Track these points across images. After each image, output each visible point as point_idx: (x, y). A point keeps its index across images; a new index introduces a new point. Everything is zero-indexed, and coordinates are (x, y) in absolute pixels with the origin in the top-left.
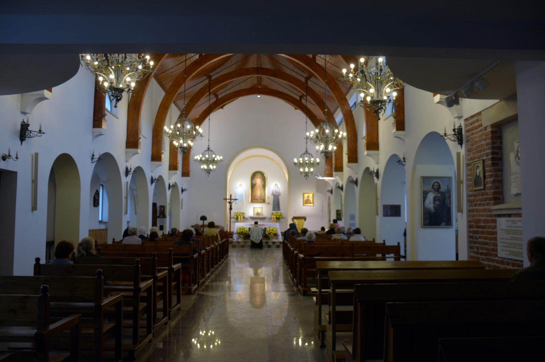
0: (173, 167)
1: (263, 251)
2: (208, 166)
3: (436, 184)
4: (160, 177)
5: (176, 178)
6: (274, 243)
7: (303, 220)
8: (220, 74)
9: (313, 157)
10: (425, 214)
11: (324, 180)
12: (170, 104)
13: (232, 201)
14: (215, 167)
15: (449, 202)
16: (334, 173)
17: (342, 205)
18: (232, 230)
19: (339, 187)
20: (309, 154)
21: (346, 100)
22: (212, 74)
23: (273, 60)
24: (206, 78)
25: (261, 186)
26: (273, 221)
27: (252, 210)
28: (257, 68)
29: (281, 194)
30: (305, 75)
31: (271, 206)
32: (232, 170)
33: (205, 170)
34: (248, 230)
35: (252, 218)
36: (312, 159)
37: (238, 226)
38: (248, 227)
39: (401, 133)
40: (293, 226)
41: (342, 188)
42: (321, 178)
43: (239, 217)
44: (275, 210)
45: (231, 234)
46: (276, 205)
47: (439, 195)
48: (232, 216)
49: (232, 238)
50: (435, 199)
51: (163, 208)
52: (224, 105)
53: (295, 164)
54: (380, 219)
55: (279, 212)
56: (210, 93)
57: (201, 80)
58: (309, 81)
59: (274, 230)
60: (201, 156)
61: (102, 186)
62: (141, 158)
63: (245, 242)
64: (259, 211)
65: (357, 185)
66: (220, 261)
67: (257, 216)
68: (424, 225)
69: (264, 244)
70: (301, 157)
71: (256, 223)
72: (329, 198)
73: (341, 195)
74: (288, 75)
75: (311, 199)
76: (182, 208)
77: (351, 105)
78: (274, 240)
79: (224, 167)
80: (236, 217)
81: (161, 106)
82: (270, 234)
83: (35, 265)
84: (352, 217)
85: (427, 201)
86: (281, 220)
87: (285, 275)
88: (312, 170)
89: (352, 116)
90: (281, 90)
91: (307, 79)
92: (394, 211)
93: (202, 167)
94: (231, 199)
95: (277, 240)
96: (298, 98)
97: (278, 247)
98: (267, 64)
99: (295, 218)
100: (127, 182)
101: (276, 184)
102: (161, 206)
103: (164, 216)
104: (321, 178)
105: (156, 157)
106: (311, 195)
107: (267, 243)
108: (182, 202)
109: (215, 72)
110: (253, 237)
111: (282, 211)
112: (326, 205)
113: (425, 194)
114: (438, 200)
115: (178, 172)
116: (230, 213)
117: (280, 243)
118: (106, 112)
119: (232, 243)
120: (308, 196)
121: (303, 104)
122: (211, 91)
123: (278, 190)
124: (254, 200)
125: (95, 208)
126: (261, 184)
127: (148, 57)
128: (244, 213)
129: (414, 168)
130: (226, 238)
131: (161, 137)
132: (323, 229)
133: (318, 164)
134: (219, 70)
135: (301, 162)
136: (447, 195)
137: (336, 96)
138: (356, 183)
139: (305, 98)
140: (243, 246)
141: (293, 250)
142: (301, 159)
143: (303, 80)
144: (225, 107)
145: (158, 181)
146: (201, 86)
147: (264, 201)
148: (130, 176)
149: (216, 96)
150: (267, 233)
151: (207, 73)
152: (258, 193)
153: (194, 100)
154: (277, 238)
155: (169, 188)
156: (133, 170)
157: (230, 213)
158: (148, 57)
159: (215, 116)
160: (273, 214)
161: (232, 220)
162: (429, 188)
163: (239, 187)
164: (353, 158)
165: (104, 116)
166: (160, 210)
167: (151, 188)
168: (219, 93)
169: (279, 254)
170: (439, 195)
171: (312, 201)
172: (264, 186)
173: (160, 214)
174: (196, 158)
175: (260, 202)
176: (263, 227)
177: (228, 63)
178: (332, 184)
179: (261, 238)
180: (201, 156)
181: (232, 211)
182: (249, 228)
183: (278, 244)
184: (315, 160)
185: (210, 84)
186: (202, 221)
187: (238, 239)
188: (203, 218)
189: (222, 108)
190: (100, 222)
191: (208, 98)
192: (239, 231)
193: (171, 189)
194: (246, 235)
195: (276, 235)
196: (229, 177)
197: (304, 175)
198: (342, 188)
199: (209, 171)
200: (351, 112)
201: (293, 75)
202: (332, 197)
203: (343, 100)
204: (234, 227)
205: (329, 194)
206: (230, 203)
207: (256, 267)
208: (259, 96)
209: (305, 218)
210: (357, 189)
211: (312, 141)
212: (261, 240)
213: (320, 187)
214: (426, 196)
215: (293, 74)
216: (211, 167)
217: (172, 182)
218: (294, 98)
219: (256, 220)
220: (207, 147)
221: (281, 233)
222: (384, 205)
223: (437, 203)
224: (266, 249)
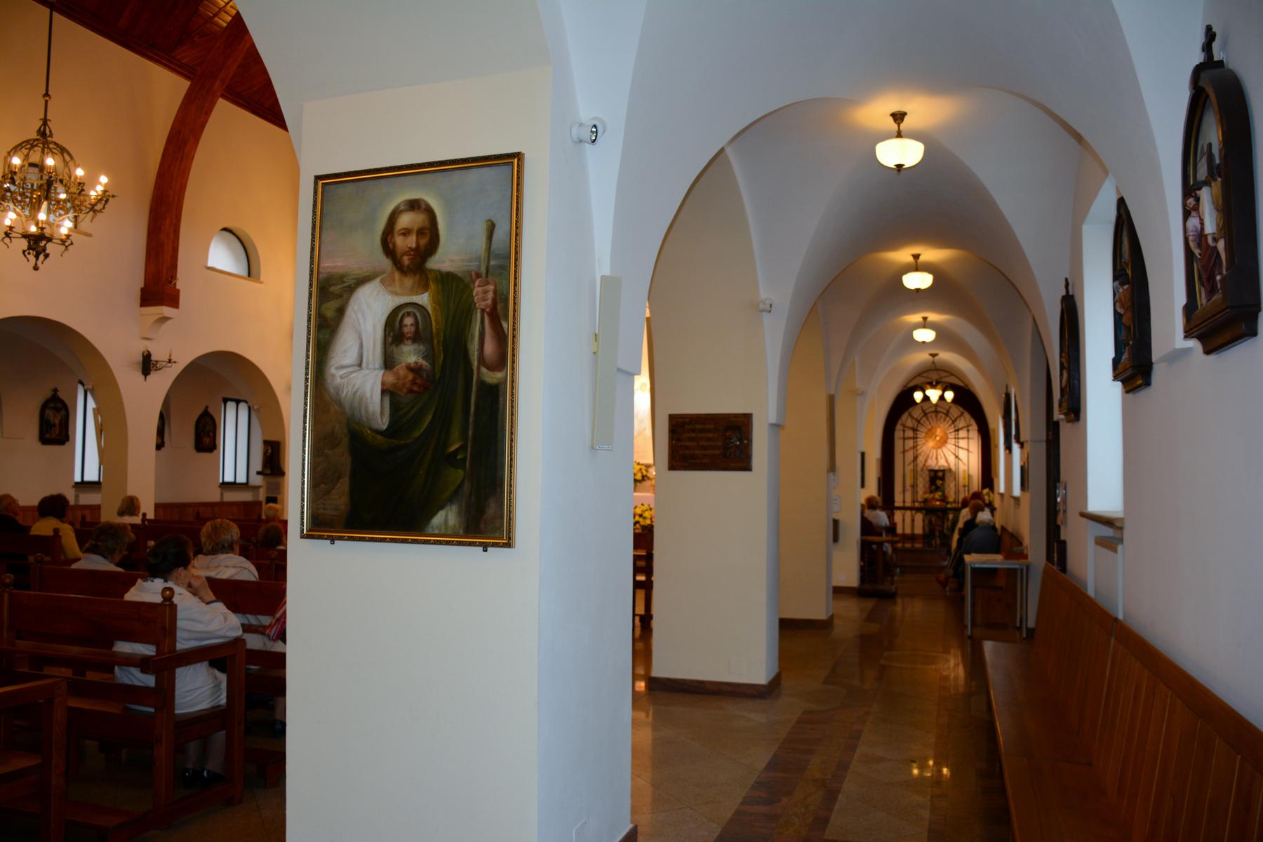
3: (405, 220)
15: (490, 348)
47: (424, 299)
50: (394, 332)
59: (647, 514)
85: (345, 351)
114: (416, 338)
125: (205, 456)
135: (332, 289)
136: (482, 295)
162: (359, 250)
170: (424, 299)
190: (225, 485)
214: (341, 312)
222: (671, 416)
223: (410, 355)
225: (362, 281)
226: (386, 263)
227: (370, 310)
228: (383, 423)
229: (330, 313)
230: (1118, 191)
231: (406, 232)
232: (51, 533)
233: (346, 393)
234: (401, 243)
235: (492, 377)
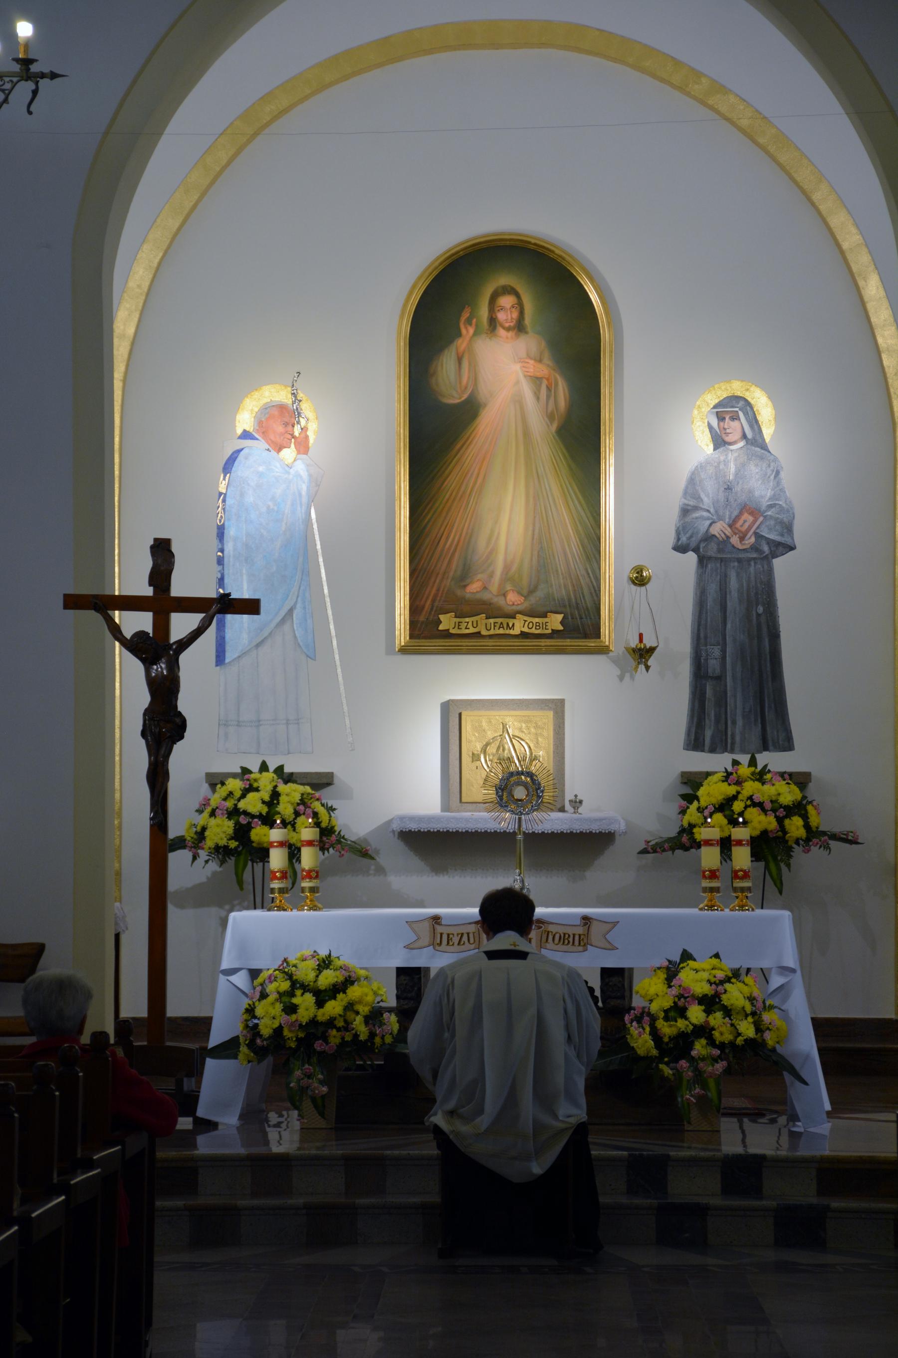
6: (743, 1173)
13: (181, 624)
18: (177, 1006)
25: (540, 427)
26: (719, 888)
27: (418, 742)
31: (669, 690)
32: (159, 236)
34: (388, 994)
35: (433, 845)
37: (255, 947)
44: (720, 745)
46: (738, 677)
48: (175, 830)
59: (735, 995)
64: (528, 743)
67: (504, 821)
69: (611, 1192)
71: (506, 912)
78: (732, 1140)
80: (220, 830)
82: (681, 1045)
86: (808, 864)
94: (162, 602)
95: (762, 1140)
101: (732, 408)
107: (648, 1173)
116: (158, 776)
119: (187, 1176)
124: (446, 612)
128: (321, 782)
140: (327, 1226)
147: (576, 627)
150: (642, 1041)
152: (508, 517)
157: (158, 776)
161: (182, 869)
163: (266, 449)
172: (580, 437)
175: (528, 644)
176: (588, 965)
179: (572, 1112)
181: (187, 762)
182: (410, 979)
183: (804, 1193)
187: (253, 1116)
189: (149, 1323)
192: (270, 1016)
194: (353, 1062)
195: (757, 1063)
196: (124, 323)
204: (215, 970)
206: (155, 650)
212: (580, 1134)
219: (513, 847)
221: (823, 1027)
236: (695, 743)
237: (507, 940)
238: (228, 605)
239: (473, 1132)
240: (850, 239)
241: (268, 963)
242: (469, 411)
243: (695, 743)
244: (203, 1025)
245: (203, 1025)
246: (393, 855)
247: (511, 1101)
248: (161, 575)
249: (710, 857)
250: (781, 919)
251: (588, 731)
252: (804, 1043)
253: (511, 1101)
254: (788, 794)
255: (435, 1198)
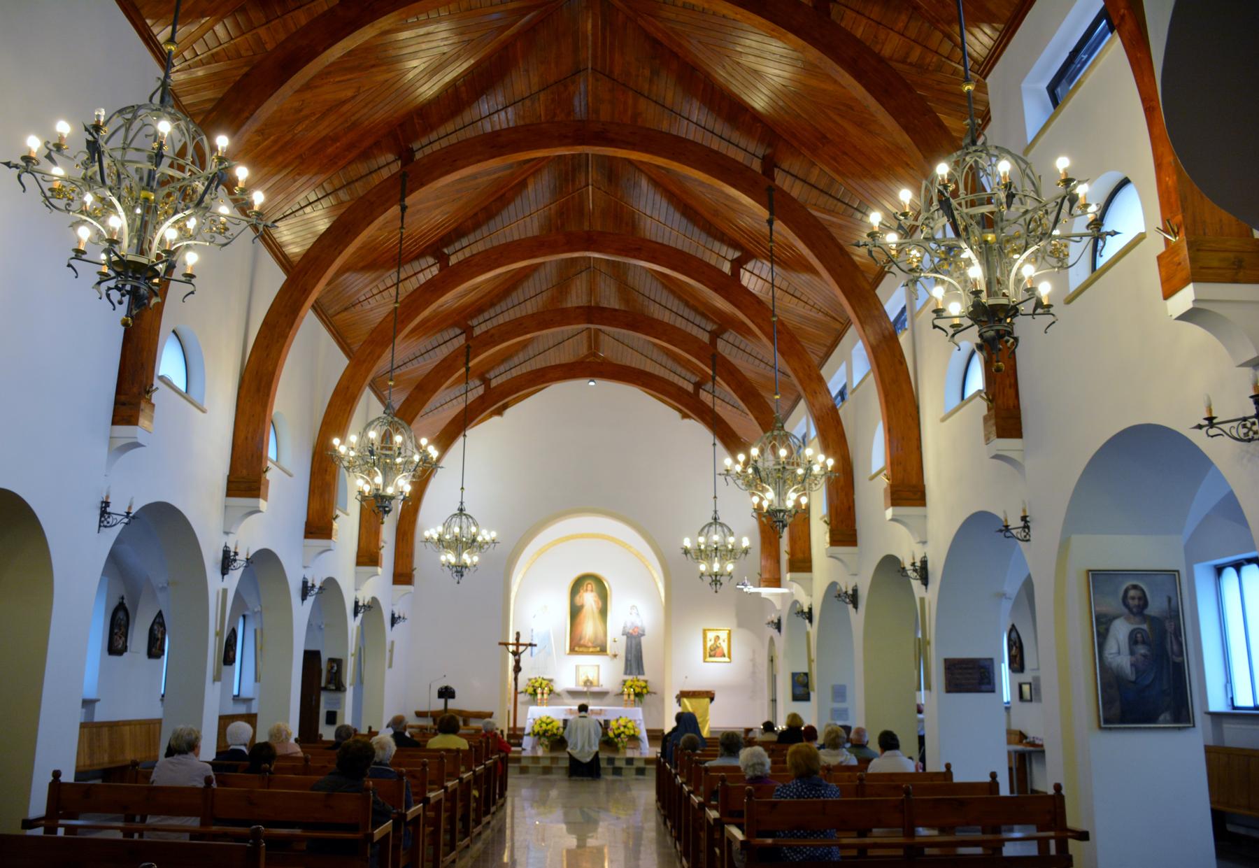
0: (367, 557)
1: (602, 785)
2: (459, 555)
3: (1132, 593)
4: (374, 600)
5: (376, 585)
6: (630, 761)
7: (708, 700)
8: (495, 322)
9: (732, 534)
10: (1106, 686)
11: (759, 594)
12: (360, 390)
13: (521, 649)
14: (476, 559)
15: (1175, 648)
16: (787, 576)
17: (810, 661)
18: (519, 725)
19: (840, 596)
20: (722, 525)
21: (820, 380)
22: (474, 322)
23: (624, 288)
24: (458, 331)
25: (596, 611)
27: (571, 672)
28: (589, 308)
29: (647, 632)
30: (694, 379)
31: (620, 664)
33: (449, 565)
34: (561, 724)
35: (573, 694)
36: (731, 540)
37: (535, 715)
38: (563, 717)
39: (1008, 445)
40: (687, 722)
41: (809, 616)
42: (751, 589)
43: (539, 691)
44: (631, 674)
45: (516, 735)
46: (634, 661)
47: (1145, 626)
48: (519, 690)
49: (520, 745)
50: (1134, 640)
51: (337, 664)
52: (505, 407)
53: (686, 552)
54: (932, 697)
55: (641, 677)
56: (468, 369)
57: (447, 338)
58: (719, 340)
59: (630, 725)
60: (440, 529)
61: (244, 617)
62: (272, 522)
63: (553, 759)
64: (592, 676)
65: (856, 607)
66: (478, 822)
68: (1106, 721)
69: (603, 764)
70: (700, 534)
71: (583, 708)
72: (772, 640)
73: (808, 634)
74: (668, 324)
75: (725, 646)
76: (390, 666)
77: (834, 393)
79: (503, 563)
80: (530, 690)
81: (336, 393)
82: (619, 736)
83: (51, 784)
84: (839, 693)
85: (1111, 647)
86: (647, 698)
87: (661, 843)
88: (730, 567)
89: (838, 422)
90: (649, 367)
91: (715, 335)
92: (969, 676)
93: (443, 558)
94: (518, 644)
96: (690, 388)
97: (640, 771)
98: (610, 298)
99: (683, 695)
100: (225, 591)
102: (331, 660)
103: (340, 688)
104: (751, 589)
105: (318, 526)
106: (723, 635)
107: (611, 761)
108: (391, 651)
109: (481, 319)
110: (576, 745)
111: (649, 674)
112: (763, 661)
113: (1102, 625)
114: (1144, 642)
115: (379, 570)
116: (516, 679)
117: (648, 761)
118: (269, 464)
120: (718, 637)
121: (703, 403)
122: (470, 364)
123: (639, 624)
124: (576, 646)
126: (594, 607)
127: (424, 441)
128: (551, 680)
129: (1064, 545)
130: (500, 751)
131: (334, 476)
132: (769, 727)
133: (746, 551)
134: (492, 312)
136: (1169, 626)
137: (794, 370)
138: (854, 598)
139: (709, 386)
140: (547, 770)
141: (702, 806)
142: (702, 540)
143: (705, 338)
144: (509, 412)
145: (325, 593)
146: (444, 352)
147: (603, 650)
148: (235, 575)
149: (486, 382)
150: (611, 734)
151: (462, 319)
152: (589, 628)
153: (423, 390)
154: (637, 747)
155: (356, 614)
156: (318, 585)
157: (516, 679)
158: (424, 441)
159: (483, 437)
160: (624, 682)
161: (521, 698)
162: (1113, 604)
163: (538, 611)
164: (844, 530)
165: (148, 392)
166: (329, 671)
167: (301, 611)
168: (492, 374)
169: (646, 794)
170: (1145, 626)
171: (726, 652)
172: (603, 612)
173: (329, 682)
174: (427, 534)
175: (593, 653)
176: (601, 719)
177: (514, 295)
178: (778, 606)
179: (596, 748)
180: (440, 529)
181: (520, 675)
182: (565, 721)
183: (641, 765)
184: (739, 541)
185: (468, 347)
186: (442, 701)
187: (534, 748)
188: (446, 693)
189: (499, 412)
190: (237, 698)
191: (462, 388)
192: (537, 729)
193: (360, 615)
194: (555, 740)
195: (634, 738)
197: (709, 580)
198: (809, 616)
199: (460, 570)
200: (834, 410)
201: (678, 325)
202: (781, 640)
203: (813, 382)
204: (526, 718)
205: (773, 632)
206: (515, 653)
207: (582, 825)
208: (592, 384)
209: (711, 696)
210: (857, 618)
211: (740, 482)
212: (597, 754)
213: (746, 612)
214: (1107, 630)
215: (680, 323)
216: (467, 558)
217: (365, 597)
218: (680, 389)
219: (585, 696)
220: (458, 505)
221: (648, 731)
222: (946, 661)
223: (1142, 650)
224: (610, 778)
225: (1115, 618)
226: (1125, 610)
227: (1121, 630)
228: (1133, 678)
229: (1102, 630)
230: (1024, 511)
231: (1133, 598)
232: (988, 779)
233: (1114, 665)
234: (1131, 602)
235: (1178, 660)
236: (626, 673)
237: (583, 714)
238: (531, 645)
239: (576, 753)
240: (656, 575)
241: (537, 717)
242: (582, 607)
243: (626, 673)
244: (523, 729)
245: (523, 729)
246: (565, 695)
247: (583, 746)
248: (517, 639)
249: (626, 697)
250: (639, 710)
251: (603, 672)
252: (644, 735)
253: (583, 746)
254: (643, 684)
255: (958, 778)
